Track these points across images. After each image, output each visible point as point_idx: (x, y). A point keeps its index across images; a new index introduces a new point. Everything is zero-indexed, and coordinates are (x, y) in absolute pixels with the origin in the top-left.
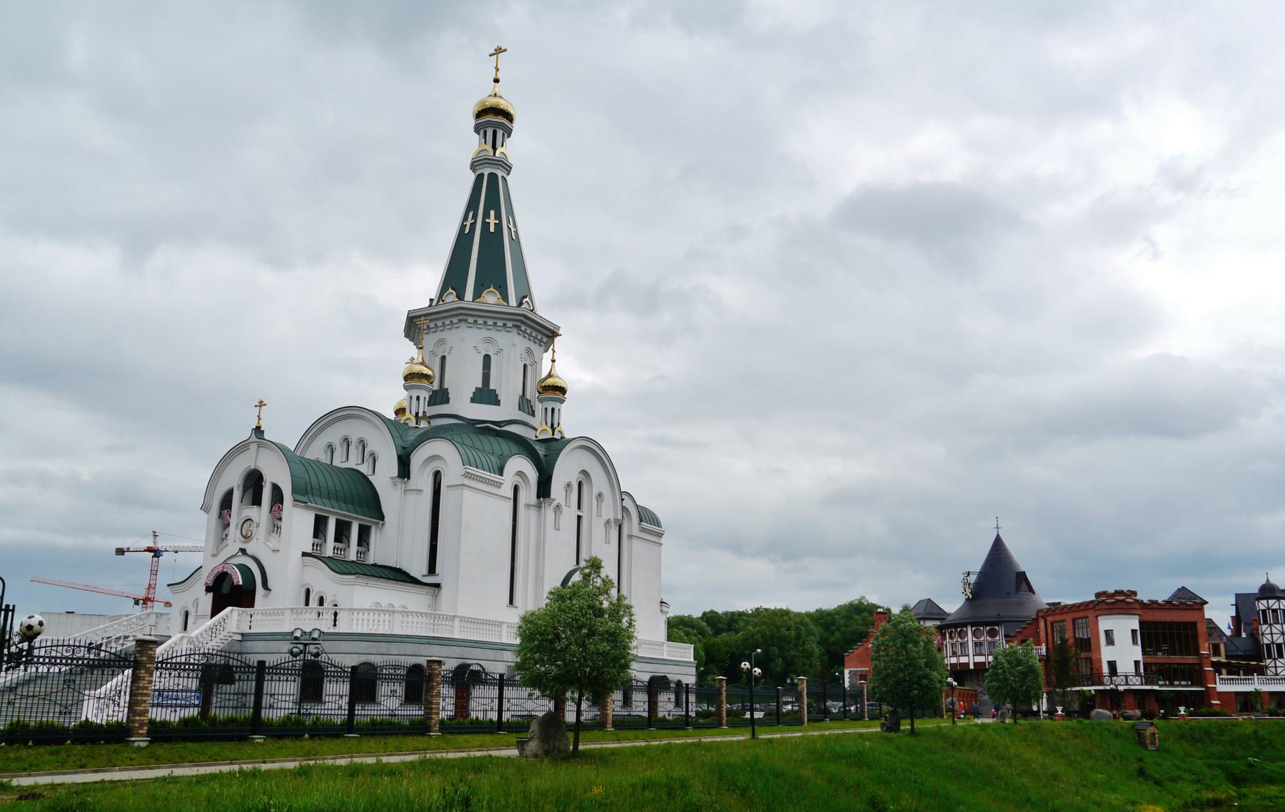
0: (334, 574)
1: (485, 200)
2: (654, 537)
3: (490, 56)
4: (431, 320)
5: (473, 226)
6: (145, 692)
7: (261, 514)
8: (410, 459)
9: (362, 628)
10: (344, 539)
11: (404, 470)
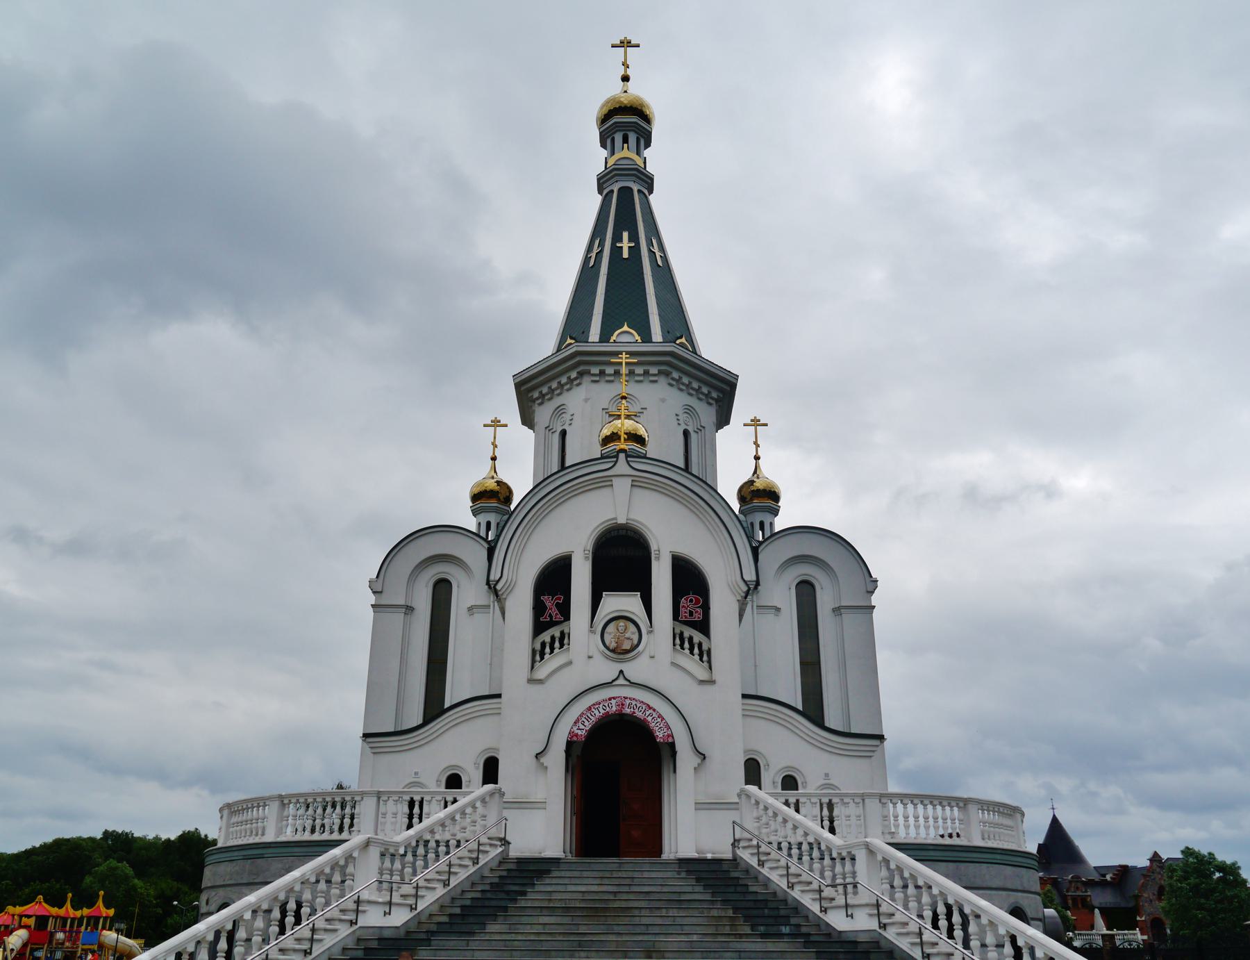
3: (612, 47)
5: (599, 254)
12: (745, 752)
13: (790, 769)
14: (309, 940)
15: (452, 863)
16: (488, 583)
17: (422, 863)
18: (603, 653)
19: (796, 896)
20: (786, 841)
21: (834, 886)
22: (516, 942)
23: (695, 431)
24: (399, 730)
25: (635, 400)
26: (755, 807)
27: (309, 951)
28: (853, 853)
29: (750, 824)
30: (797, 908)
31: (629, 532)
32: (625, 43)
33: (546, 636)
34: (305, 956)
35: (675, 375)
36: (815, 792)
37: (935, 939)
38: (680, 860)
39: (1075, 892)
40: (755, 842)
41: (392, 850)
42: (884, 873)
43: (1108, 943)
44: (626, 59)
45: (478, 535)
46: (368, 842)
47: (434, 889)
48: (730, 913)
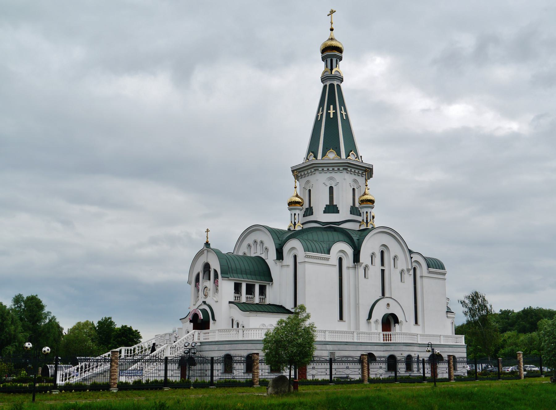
0: (241, 311)
2: (438, 275)
3: (328, 16)
4: (299, 172)
5: (322, 115)
6: (115, 371)
7: (210, 284)
8: (282, 250)
9: (256, 337)
10: (253, 293)
11: (280, 256)
41: (173, 347)
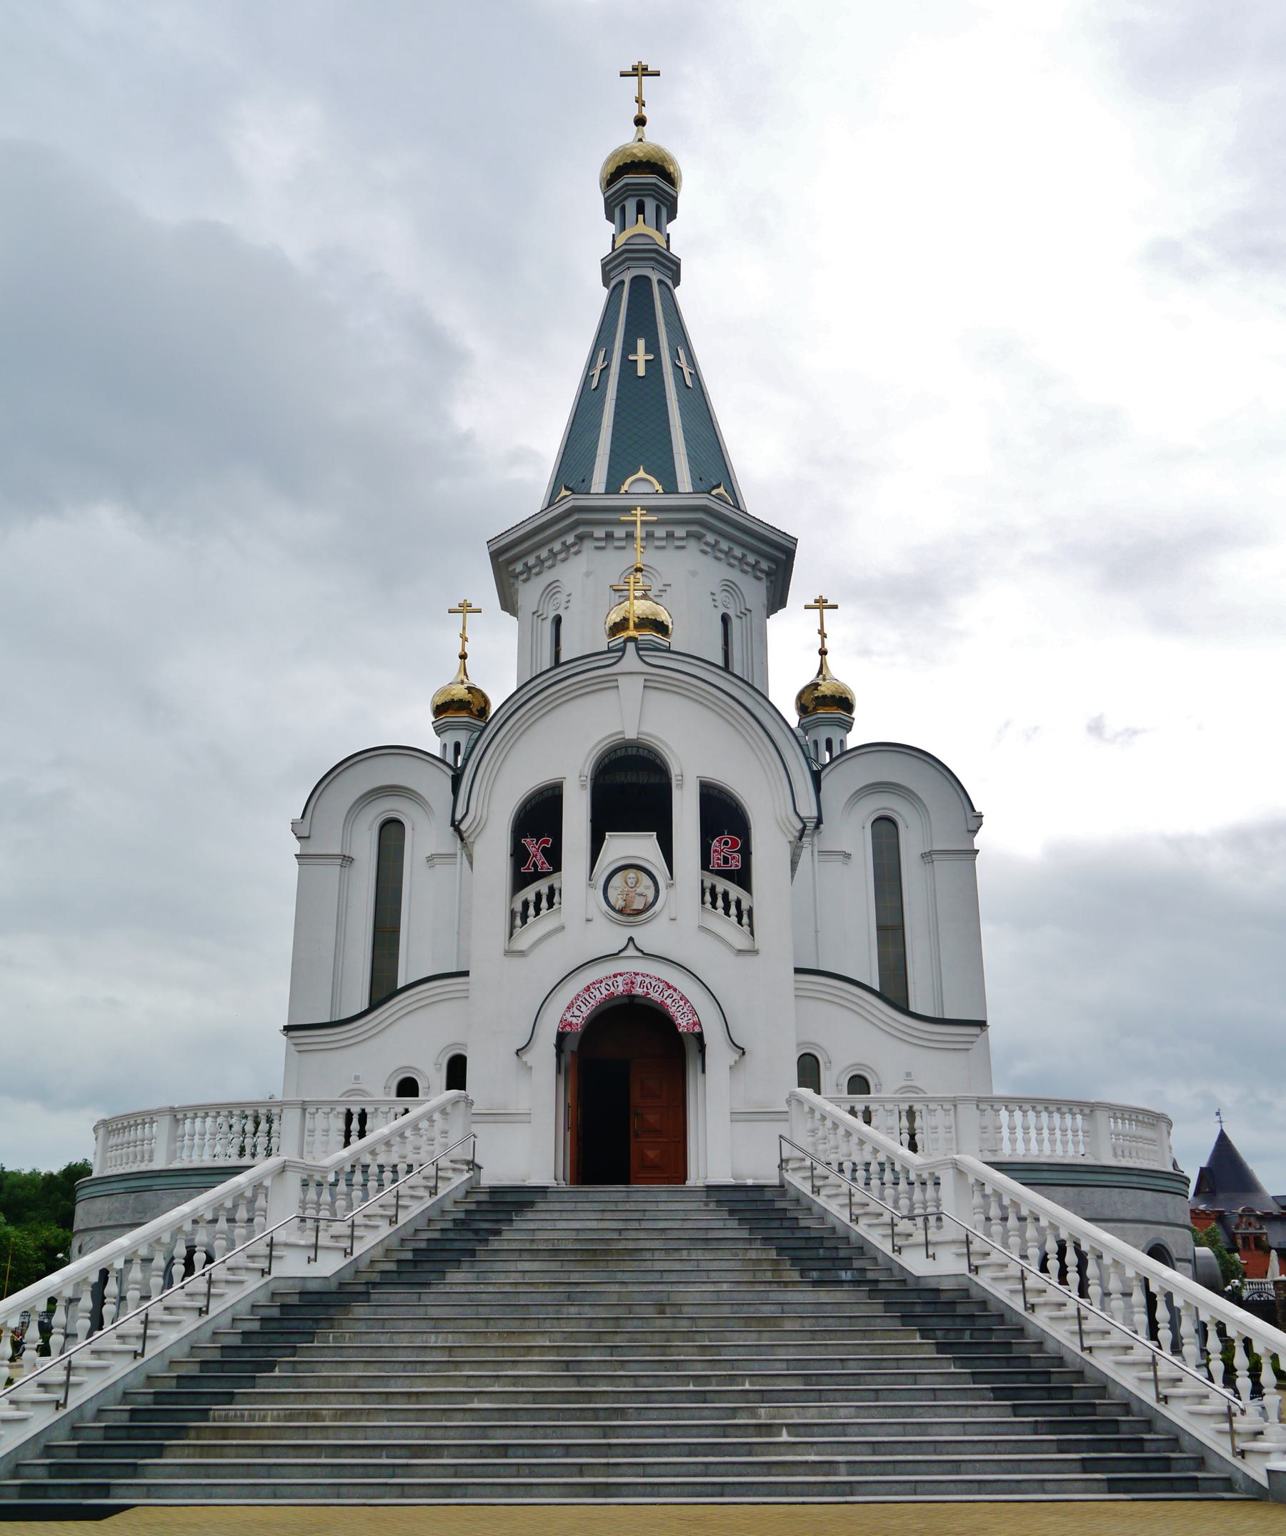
1: (628, 309)
3: (621, 75)
5: (606, 369)
12: (798, 1045)
13: (862, 1067)
14: (205, 1294)
15: (400, 1194)
16: (453, 824)
17: (360, 1194)
18: (606, 915)
19: (860, 1232)
20: (850, 1160)
21: (912, 1218)
22: (484, 1295)
23: (737, 616)
24: (337, 1019)
25: (656, 574)
26: (809, 1116)
27: (204, 1309)
28: (937, 1174)
29: (803, 1140)
30: (862, 1248)
31: (641, 751)
32: (640, 70)
33: (529, 893)
34: (200, 1315)
35: (710, 538)
36: (893, 1096)
37: (1042, 1285)
38: (707, 1187)
39: (1247, 1229)
40: (808, 1163)
41: (317, 1177)
42: (977, 1199)
43: (1282, 1292)
44: (640, 94)
45: (442, 761)
46: (284, 1167)
47: (376, 1227)
48: (773, 1255)
